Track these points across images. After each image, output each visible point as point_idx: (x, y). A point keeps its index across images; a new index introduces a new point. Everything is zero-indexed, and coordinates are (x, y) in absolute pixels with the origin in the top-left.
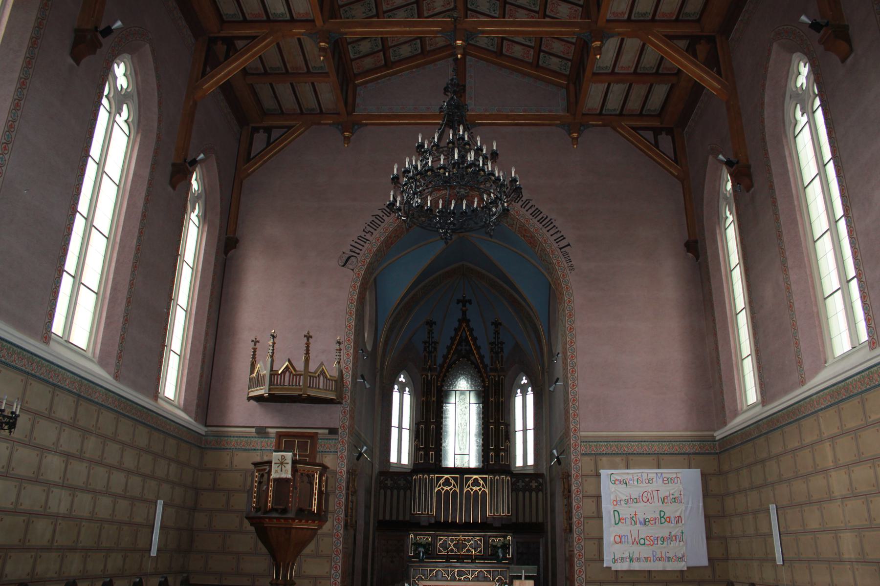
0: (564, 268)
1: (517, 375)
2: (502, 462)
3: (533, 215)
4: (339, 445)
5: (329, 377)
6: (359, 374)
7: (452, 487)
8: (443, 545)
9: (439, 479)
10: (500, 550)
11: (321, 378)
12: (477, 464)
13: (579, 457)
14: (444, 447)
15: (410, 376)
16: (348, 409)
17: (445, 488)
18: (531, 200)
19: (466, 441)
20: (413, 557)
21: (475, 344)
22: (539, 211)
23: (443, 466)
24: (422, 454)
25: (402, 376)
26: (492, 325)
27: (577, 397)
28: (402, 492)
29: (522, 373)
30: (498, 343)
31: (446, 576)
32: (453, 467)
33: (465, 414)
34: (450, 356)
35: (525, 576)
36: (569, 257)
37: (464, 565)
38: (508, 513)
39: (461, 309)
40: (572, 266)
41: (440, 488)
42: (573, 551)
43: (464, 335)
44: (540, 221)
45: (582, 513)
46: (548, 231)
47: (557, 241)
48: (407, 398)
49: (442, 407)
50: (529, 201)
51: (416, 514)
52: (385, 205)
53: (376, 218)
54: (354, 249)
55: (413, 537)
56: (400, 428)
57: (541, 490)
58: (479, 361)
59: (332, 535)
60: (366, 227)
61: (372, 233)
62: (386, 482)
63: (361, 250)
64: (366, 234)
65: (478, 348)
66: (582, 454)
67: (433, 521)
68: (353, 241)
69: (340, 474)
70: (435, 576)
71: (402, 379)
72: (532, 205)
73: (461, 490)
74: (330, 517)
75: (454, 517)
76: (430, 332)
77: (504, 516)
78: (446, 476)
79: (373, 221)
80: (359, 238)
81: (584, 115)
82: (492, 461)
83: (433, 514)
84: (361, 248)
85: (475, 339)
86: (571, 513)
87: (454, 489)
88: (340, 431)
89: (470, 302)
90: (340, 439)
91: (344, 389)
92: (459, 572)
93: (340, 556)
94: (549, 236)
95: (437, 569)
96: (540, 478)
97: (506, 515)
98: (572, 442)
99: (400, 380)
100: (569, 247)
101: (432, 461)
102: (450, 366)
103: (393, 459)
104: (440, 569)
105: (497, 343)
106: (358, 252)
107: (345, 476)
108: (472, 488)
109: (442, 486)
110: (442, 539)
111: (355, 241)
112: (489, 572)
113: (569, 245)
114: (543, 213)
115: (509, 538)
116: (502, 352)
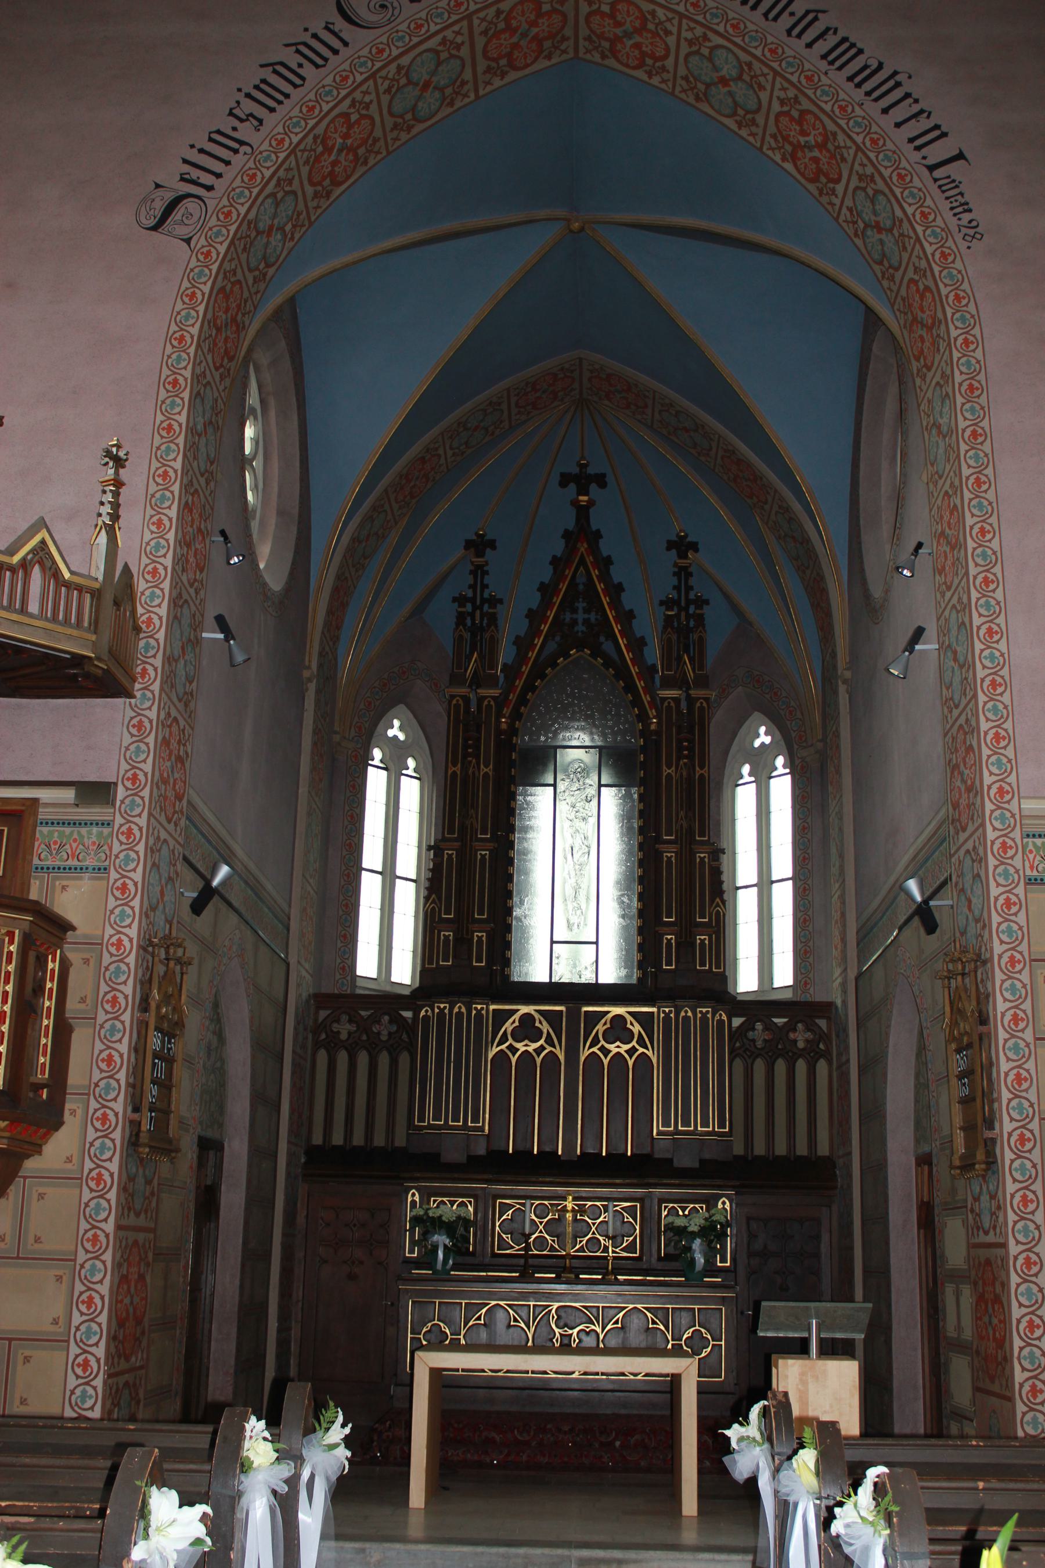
0: (946, 229)
1: (740, 721)
2: (703, 964)
3: (830, 58)
4: (116, 843)
5: (67, 575)
6: (210, 614)
7: (542, 1042)
8: (515, 1225)
9: (501, 1017)
10: (697, 1244)
11: (36, 572)
12: (623, 972)
13: (1020, 890)
14: (519, 919)
15: (421, 721)
16: (153, 714)
17: (521, 1047)
18: (824, 12)
19: (588, 899)
20: (417, 1264)
21: (616, 604)
22: (853, 45)
23: (516, 978)
24: (447, 937)
25: (396, 723)
26: (668, 549)
27: (1005, 672)
28: (384, 1060)
29: (757, 715)
30: (689, 602)
31: (523, 1325)
32: (548, 980)
33: (584, 819)
34: (538, 642)
35: (821, 1342)
36: (952, 209)
37: (579, 1288)
38: (722, 1125)
39: (575, 503)
40: (972, 225)
41: (503, 1047)
42: (1004, 1245)
43: (581, 579)
44: (857, 80)
45: (1034, 1099)
46: (885, 111)
47: (919, 142)
48: (411, 790)
49: (513, 796)
50: (813, 15)
51: (430, 1127)
52: (306, 30)
53: (275, 72)
54: (195, 174)
55: (417, 1198)
56: (389, 874)
57: (827, 1055)
58: (628, 656)
59: (77, 1180)
60: (238, 103)
61: (261, 122)
62: (335, 1027)
63: (219, 176)
64: (236, 123)
65: (627, 617)
66: (1030, 882)
67: (481, 1150)
68: (192, 146)
69: (113, 950)
70: (485, 1325)
71: (395, 731)
72: (828, 29)
73: (572, 1053)
74: (73, 1112)
75: (548, 1134)
76: (479, 572)
77: (708, 1133)
78: (524, 1009)
79: (264, 81)
80: (215, 136)
81: (802, 1446)
82: (669, 963)
83: (482, 1129)
84: (218, 171)
85: (616, 590)
86: (992, 1102)
87: (549, 1049)
88: (121, 793)
89: (601, 480)
90: (119, 820)
91: (142, 643)
92: (563, 1314)
93: (108, 1257)
94: (890, 129)
95: (493, 1303)
96: (819, 1017)
97: (713, 1133)
98: (991, 835)
99: (391, 733)
100: (961, 162)
101: (479, 960)
102: (538, 672)
103: (366, 965)
104: (502, 1303)
105: (683, 604)
106: (209, 183)
107: (131, 960)
108: (607, 1046)
109: (510, 1041)
110: (511, 1206)
111: (198, 146)
112: (662, 1314)
113: (960, 156)
114: (867, 53)
115: (724, 1204)
116: (701, 628)
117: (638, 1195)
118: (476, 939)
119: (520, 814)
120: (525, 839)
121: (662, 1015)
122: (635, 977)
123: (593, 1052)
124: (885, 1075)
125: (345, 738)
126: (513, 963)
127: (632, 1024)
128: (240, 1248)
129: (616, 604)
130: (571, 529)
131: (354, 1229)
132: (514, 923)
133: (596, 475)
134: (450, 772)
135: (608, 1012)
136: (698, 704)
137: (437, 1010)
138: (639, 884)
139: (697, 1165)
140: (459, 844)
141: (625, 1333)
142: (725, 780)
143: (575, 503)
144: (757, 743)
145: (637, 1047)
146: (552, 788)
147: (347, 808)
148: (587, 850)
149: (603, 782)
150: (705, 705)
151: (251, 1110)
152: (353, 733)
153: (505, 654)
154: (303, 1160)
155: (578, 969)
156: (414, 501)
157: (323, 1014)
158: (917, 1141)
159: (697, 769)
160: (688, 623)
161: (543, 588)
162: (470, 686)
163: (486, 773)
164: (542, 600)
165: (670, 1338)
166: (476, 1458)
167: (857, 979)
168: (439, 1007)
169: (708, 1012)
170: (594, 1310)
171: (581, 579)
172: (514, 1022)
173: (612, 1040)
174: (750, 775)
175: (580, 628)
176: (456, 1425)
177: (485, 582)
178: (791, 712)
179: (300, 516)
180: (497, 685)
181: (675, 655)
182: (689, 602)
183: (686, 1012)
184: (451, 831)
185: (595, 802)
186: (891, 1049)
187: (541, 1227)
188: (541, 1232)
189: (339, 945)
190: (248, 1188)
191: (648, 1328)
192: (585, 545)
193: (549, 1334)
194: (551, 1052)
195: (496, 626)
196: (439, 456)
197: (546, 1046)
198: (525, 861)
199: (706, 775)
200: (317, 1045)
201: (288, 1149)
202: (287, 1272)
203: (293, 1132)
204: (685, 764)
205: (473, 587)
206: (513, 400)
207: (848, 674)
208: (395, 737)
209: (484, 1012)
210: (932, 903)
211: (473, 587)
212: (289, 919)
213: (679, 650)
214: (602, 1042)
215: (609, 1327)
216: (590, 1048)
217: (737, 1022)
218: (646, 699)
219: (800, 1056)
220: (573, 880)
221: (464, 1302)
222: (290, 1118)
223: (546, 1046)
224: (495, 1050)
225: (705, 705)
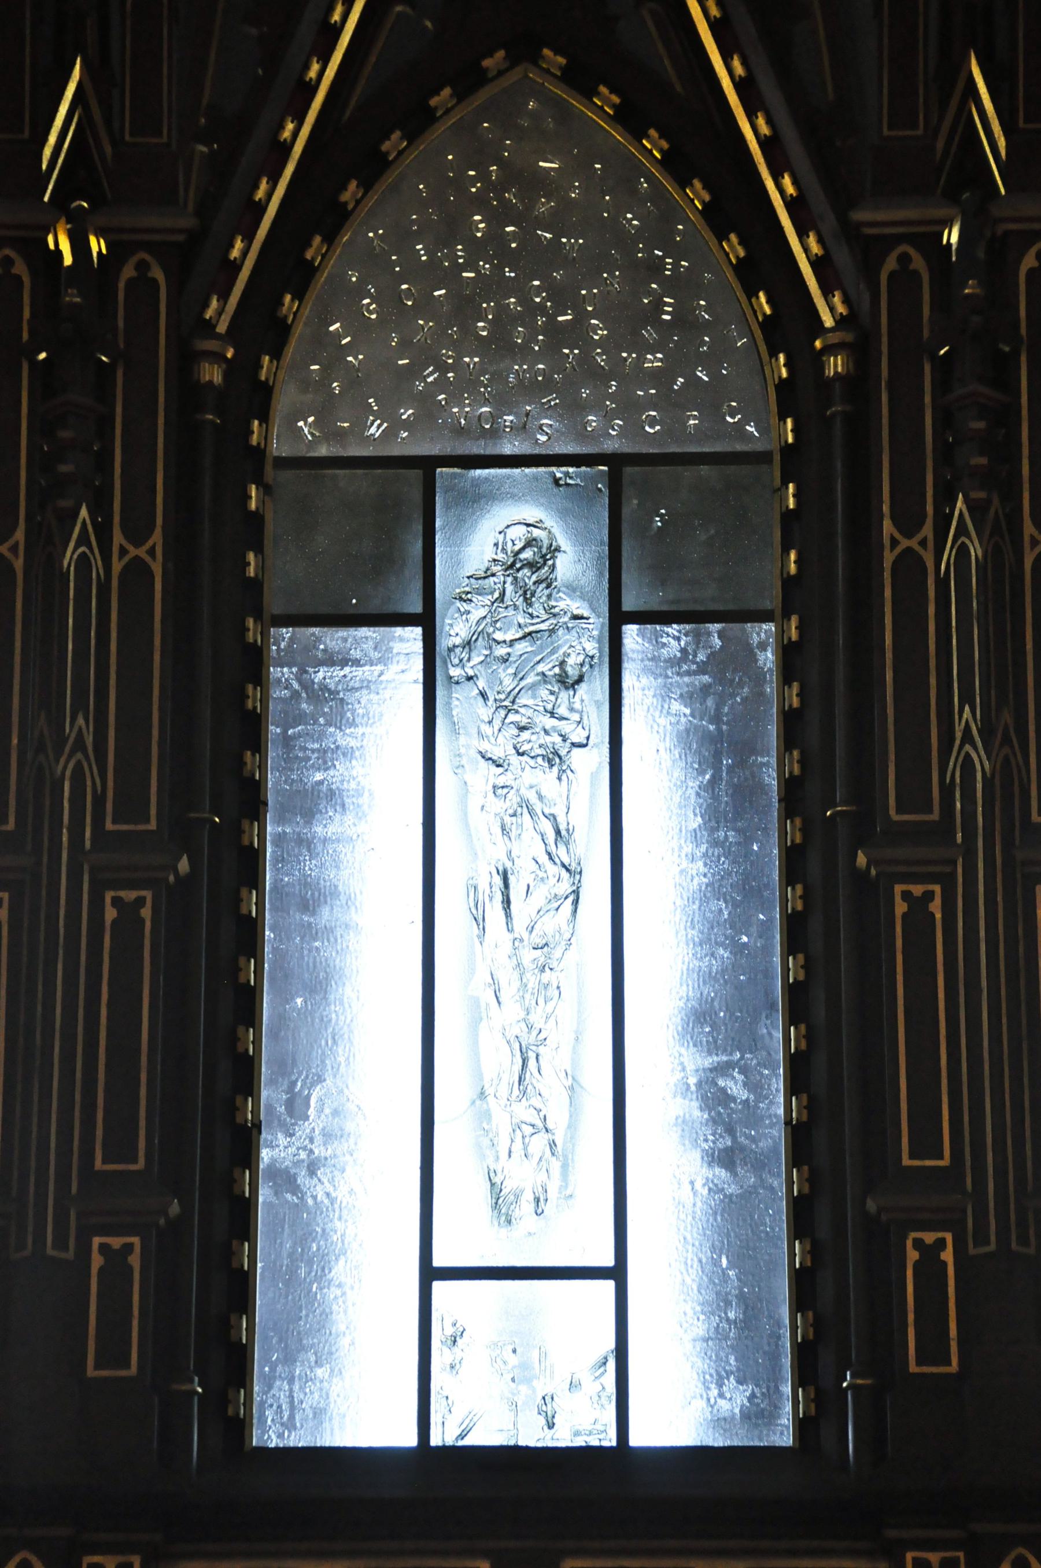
14: (286, 1180)
32: (409, 1439)
33: (553, 758)
119: (287, 742)
120: (306, 843)
122: (786, 1419)
126: (260, 1368)
132: (264, 1194)
148: (565, 886)
149: (628, 604)
155: (542, 1388)
185: (598, 686)
198: (310, 932)
220: (512, 1011)
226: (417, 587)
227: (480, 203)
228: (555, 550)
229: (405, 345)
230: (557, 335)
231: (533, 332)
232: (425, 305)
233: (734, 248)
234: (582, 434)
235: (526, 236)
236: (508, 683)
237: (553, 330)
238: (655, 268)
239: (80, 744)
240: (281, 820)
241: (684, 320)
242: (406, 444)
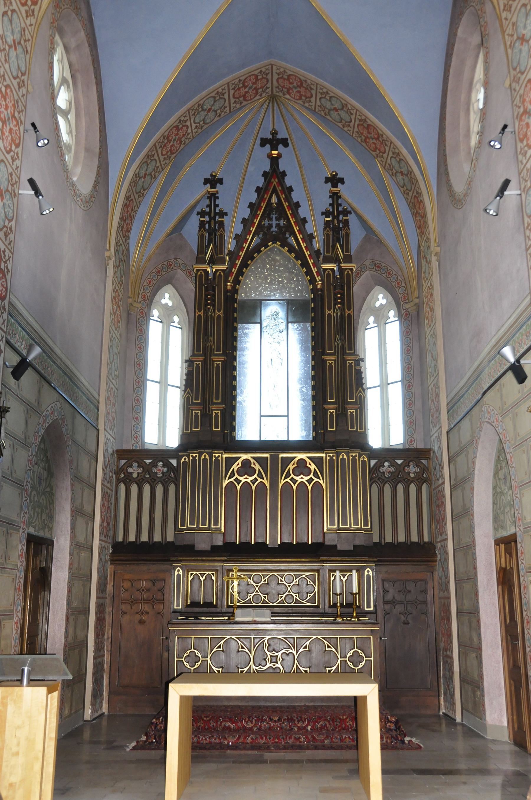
2: (352, 427)
7: (255, 476)
9: (230, 462)
12: (304, 433)
14: (240, 403)
17: (243, 479)
24: (196, 414)
25: (167, 295)
26: (326, 182)
29: (377, 287)
31: (247, 650)
34: (249, 238)
38: (366, 524)
39: (270, 156)
41: (232, 480)
43: (274, 200)
49: (235, 329)
55: (181, 573)
56: (163, 383)
58: (303, 245)
62: (130, 470)
67: (219, 542)
70: (223, 651)
73: (274, 482)
76: (213, 197)
77: (358, 529)
78: (245, 456)
82: (332, 427)
87: (260, 480)
89: (285, 142)
95: (228, 637)
99: (163, 301)
102: (250, 256)
104: (233, 637)
116: (347, 228)
117: (316, 568)
118: (214, 414)
119: (240, 340)
121: (328, 458)
122: (311, 436)
123: (287, 482)
124: (472, 489)
125: (135, 301)
126: (237, 429)
127: (310, 464)
128: (65, 607)
129: (295, 214)
130: (268, 171)
131: (143, 593)
132: (237, 405)
133: (282, 139)
134: (197, 315)
135: (295, 457)
136: (346, 272)
137: (191, 458)
138: (313, 380)
139: (352, 549)
140: (203, 357)
141: (311, 654)
142: (359, 327)
143: (270, 156)
144: (377, 304)
145: (313, 478)
146: (259, 325)
147: (137, 343)
148: (280, 361)
149: (289, 321)
150: (350, 272)
151: (72, 519)
152: (140, 299)
153: (230, 245)
154: (111, 551)
156: (173, 156)
157: (123, 462)
158: (496, 529)
159: (346, 310)
160: (339, 225)
161: (251, 206)
162: (209, 264)
163: (219, 315)
164: (251, 212)
165: (339, 656)
166: (217, 741)
167: (447, 433)
168: (192, 456)
169: (356, 456)
170: (291, 640)
171: (274, 200)
172: (238, 464)
173: (297, 474)
174: (374, 323)
175: (274, 229)
176: (205, 719)
177: (217, 203)
178: (398, 283)
179: (100, 153)
180: (225, 263)
181: (331, 244)
182: (339, 213)
183: (343, 456)
184: (198, 350)
186: (476, 472)
187: (257, 589)
188: (257, 592)
189: (134, 423)
190: (70, 569)
191: (325, 651)
192: (277, 180)
193: (263, 656)
194: (261, 482)
195: (224, 229)
196: (187, 127)
197: (258, 478)
198: (244, 368)
199: (352, 314)
200: (119, 481)
201: (100, 544)
202: (100, 621)
203: (104, 534)
204: (339, 307)
205: (209, 206)
206: (232, 92)
207: (438, 249)
208: (166, 304)
209: (220, 458)
210: (522, 362)
211: (209, 206)
212: (99, 403)
213: (333, 241)
214: (292, 476)
215: (301, 650)
216: (284, 479)
217: (373, 462)
218: (314, 270)
219: (412, 482)
221: (209, 637)
222: (101, 525)
223: (258, 478)
224: (227, 481)
225: (350, 272)
226: (259, 318)
227: (268, 263)
228: (279, 313)
229: (257, 284)
230: (279, 282)
231: (276, 281)
232: (260, 278)
233: (305, 270)
234: (283, 296)
235: (275, 268)
236: (272, 332)
237: (279, 281)
238: (293, 273)
239: (211, 341)
240: (239, 352)
241: (298, 280)
242: (258, 298)
